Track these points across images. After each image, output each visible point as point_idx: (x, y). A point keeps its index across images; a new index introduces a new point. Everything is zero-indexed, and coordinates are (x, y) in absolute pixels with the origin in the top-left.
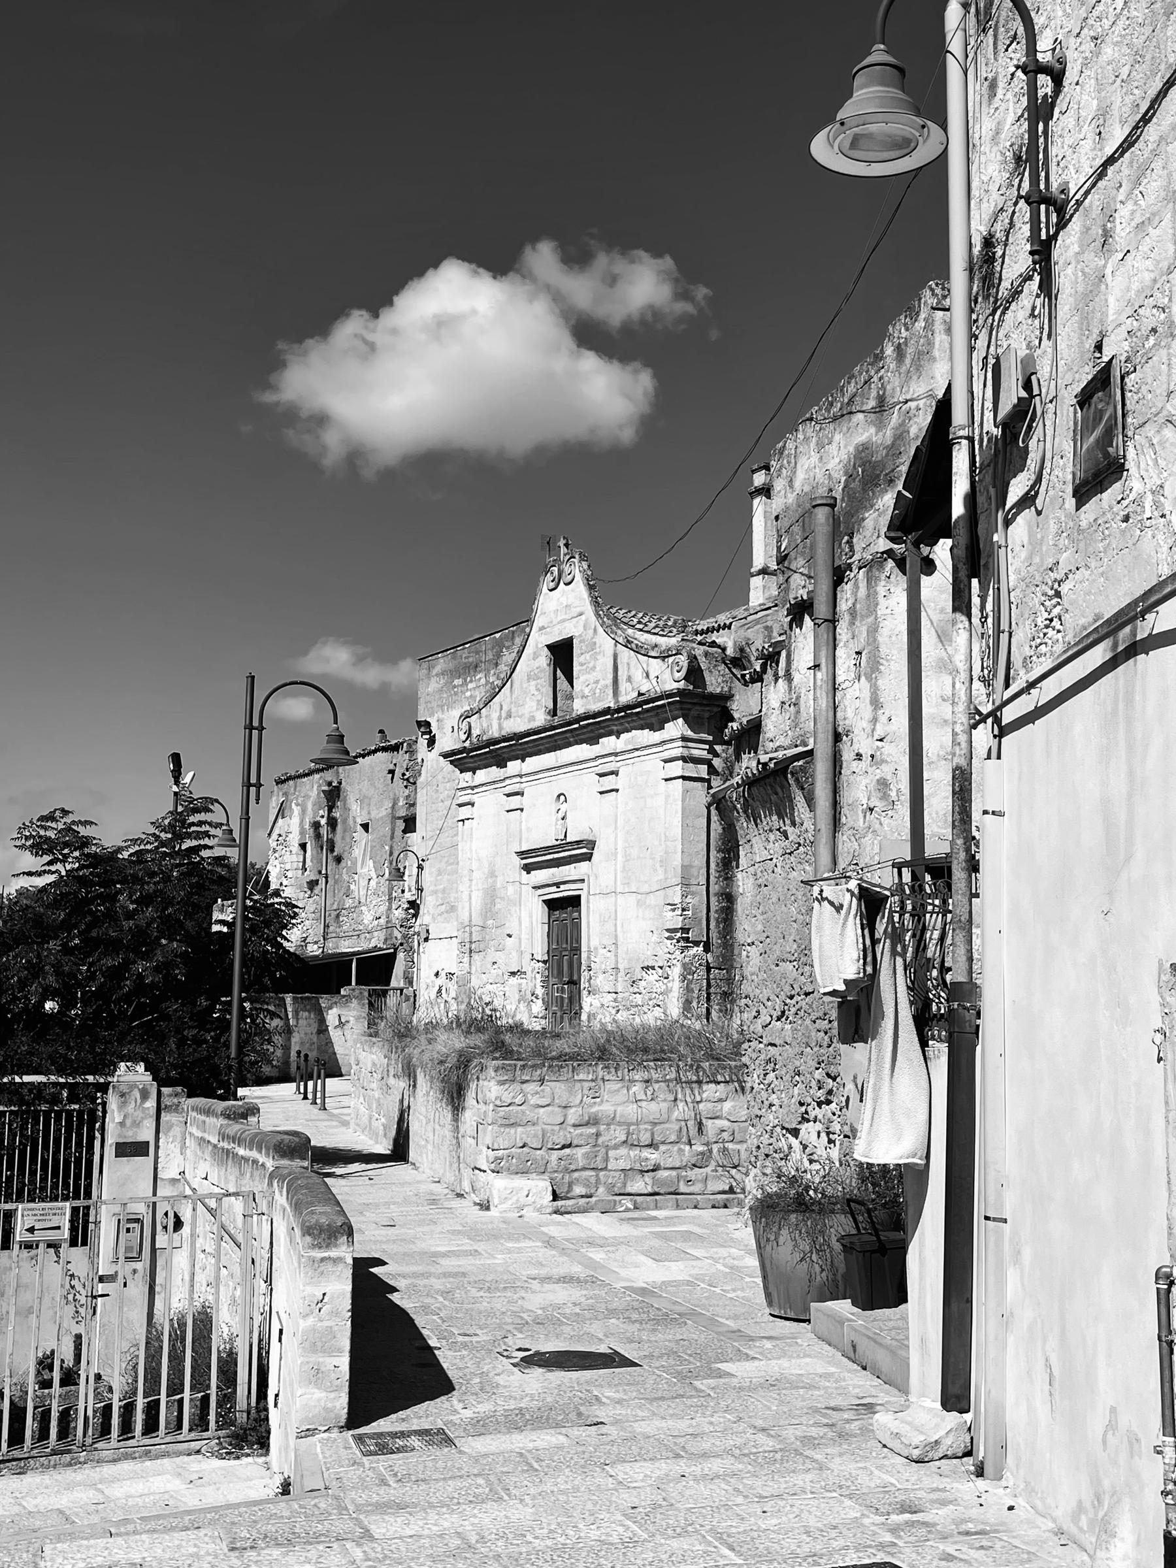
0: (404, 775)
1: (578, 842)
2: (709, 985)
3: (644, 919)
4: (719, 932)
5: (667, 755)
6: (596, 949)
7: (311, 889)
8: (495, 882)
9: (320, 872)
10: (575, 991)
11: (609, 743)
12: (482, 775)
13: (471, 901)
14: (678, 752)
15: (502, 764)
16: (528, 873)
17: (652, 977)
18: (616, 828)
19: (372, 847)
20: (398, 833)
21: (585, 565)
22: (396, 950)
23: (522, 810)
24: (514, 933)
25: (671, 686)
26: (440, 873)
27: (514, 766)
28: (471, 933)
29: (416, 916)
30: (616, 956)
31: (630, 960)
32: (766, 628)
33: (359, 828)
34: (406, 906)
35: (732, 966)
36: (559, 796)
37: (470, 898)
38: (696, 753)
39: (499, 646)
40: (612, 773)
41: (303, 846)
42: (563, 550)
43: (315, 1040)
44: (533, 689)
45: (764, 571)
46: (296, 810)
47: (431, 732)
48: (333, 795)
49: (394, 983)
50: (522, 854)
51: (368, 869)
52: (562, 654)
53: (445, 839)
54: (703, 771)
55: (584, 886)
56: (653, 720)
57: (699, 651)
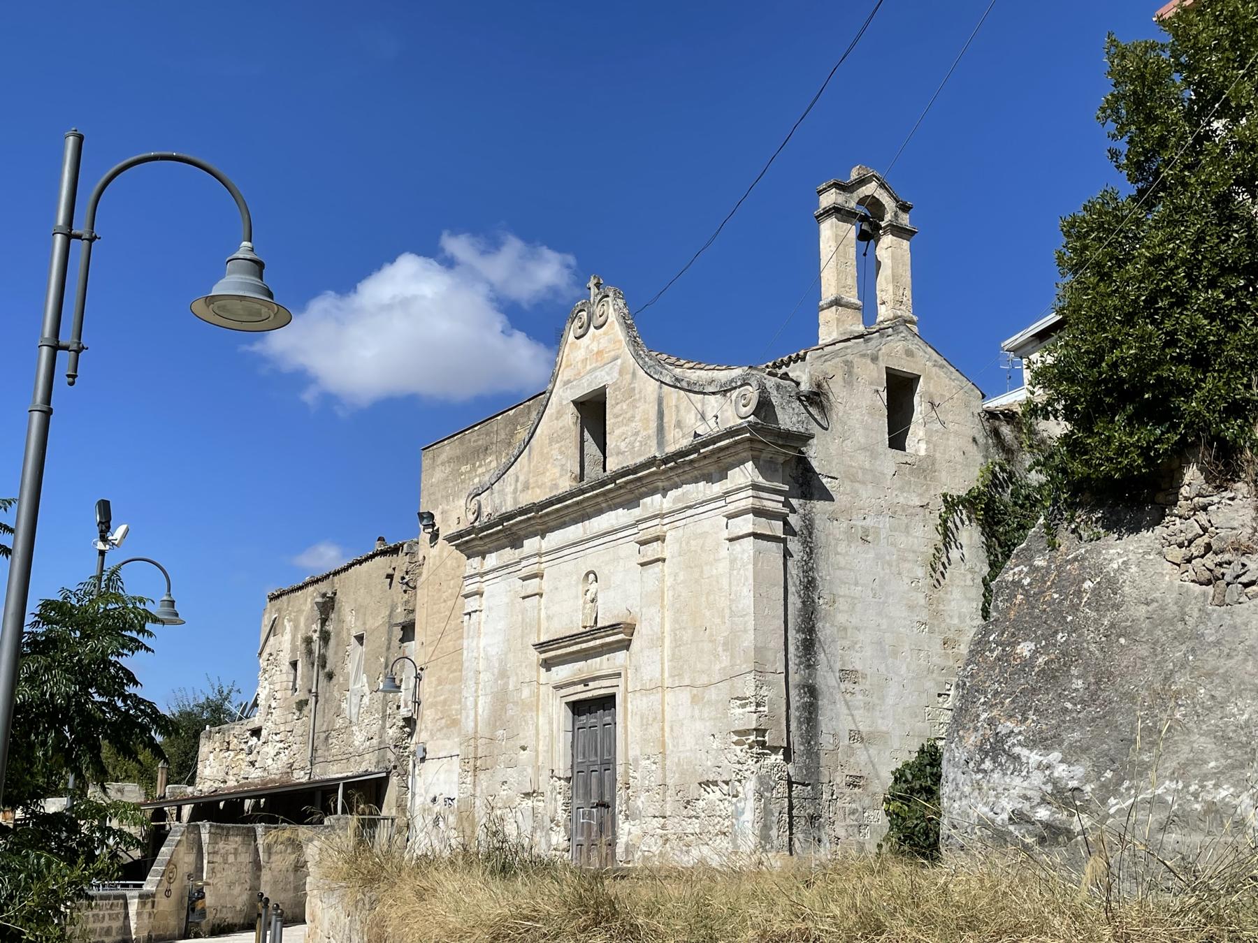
0: (403, 578)
1: (613, 626)
2: (791, 807)
3: (702, 719)
4: (801, 736)
5: (732, 508)
6: (636, 760)
7: (300, 710)
8: (507, 684)
9: (310, 691)
10: (607, 817)
11: (654, 503)
12: (492, 560)
13: (476, 707)
14: (749, 503)
15: (516, 543)
16: (548, 670)
17: (714, 795)
18: (662, 607)
19: (366, 660)
20: (395, 642)
21: (621, 303)
22: (389, 773)
23: (541, 595)
24: (530, 743)
25: (734, 422)
26: (440, 682)
27: (531, 544)
28: (476, 747)
29: (410, 735)
30: (663, 768)
31: (682, 773)
32: (846, 362)
33: (353, 640)
34: (401, 723)
35: (818, 782)
36: (587, 575)
37: (476, 705)
38: (770, 505)
39: (514, 423)
40: (657, 539)
41: (294, 665)
42: (594, 290)
43: (292, 878)
44: (555, 453)
45: (837, 302)
46: (288, 626)
47: (433, 525)
48: (327, 607)
49: (385, 812)
50: (541, 646)
51: (361, 684)
52: (592, 411)
53: (448, 644)
54: (777, 528)
55: (621, 681)
56: (712, 469)
57: (771, 382)
